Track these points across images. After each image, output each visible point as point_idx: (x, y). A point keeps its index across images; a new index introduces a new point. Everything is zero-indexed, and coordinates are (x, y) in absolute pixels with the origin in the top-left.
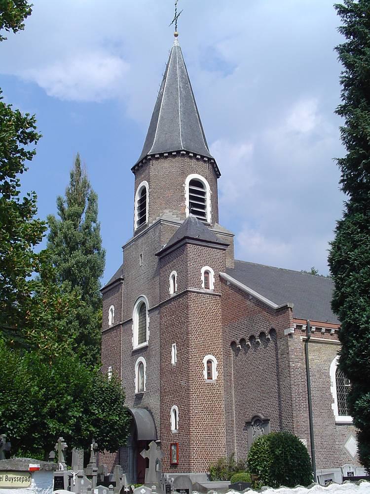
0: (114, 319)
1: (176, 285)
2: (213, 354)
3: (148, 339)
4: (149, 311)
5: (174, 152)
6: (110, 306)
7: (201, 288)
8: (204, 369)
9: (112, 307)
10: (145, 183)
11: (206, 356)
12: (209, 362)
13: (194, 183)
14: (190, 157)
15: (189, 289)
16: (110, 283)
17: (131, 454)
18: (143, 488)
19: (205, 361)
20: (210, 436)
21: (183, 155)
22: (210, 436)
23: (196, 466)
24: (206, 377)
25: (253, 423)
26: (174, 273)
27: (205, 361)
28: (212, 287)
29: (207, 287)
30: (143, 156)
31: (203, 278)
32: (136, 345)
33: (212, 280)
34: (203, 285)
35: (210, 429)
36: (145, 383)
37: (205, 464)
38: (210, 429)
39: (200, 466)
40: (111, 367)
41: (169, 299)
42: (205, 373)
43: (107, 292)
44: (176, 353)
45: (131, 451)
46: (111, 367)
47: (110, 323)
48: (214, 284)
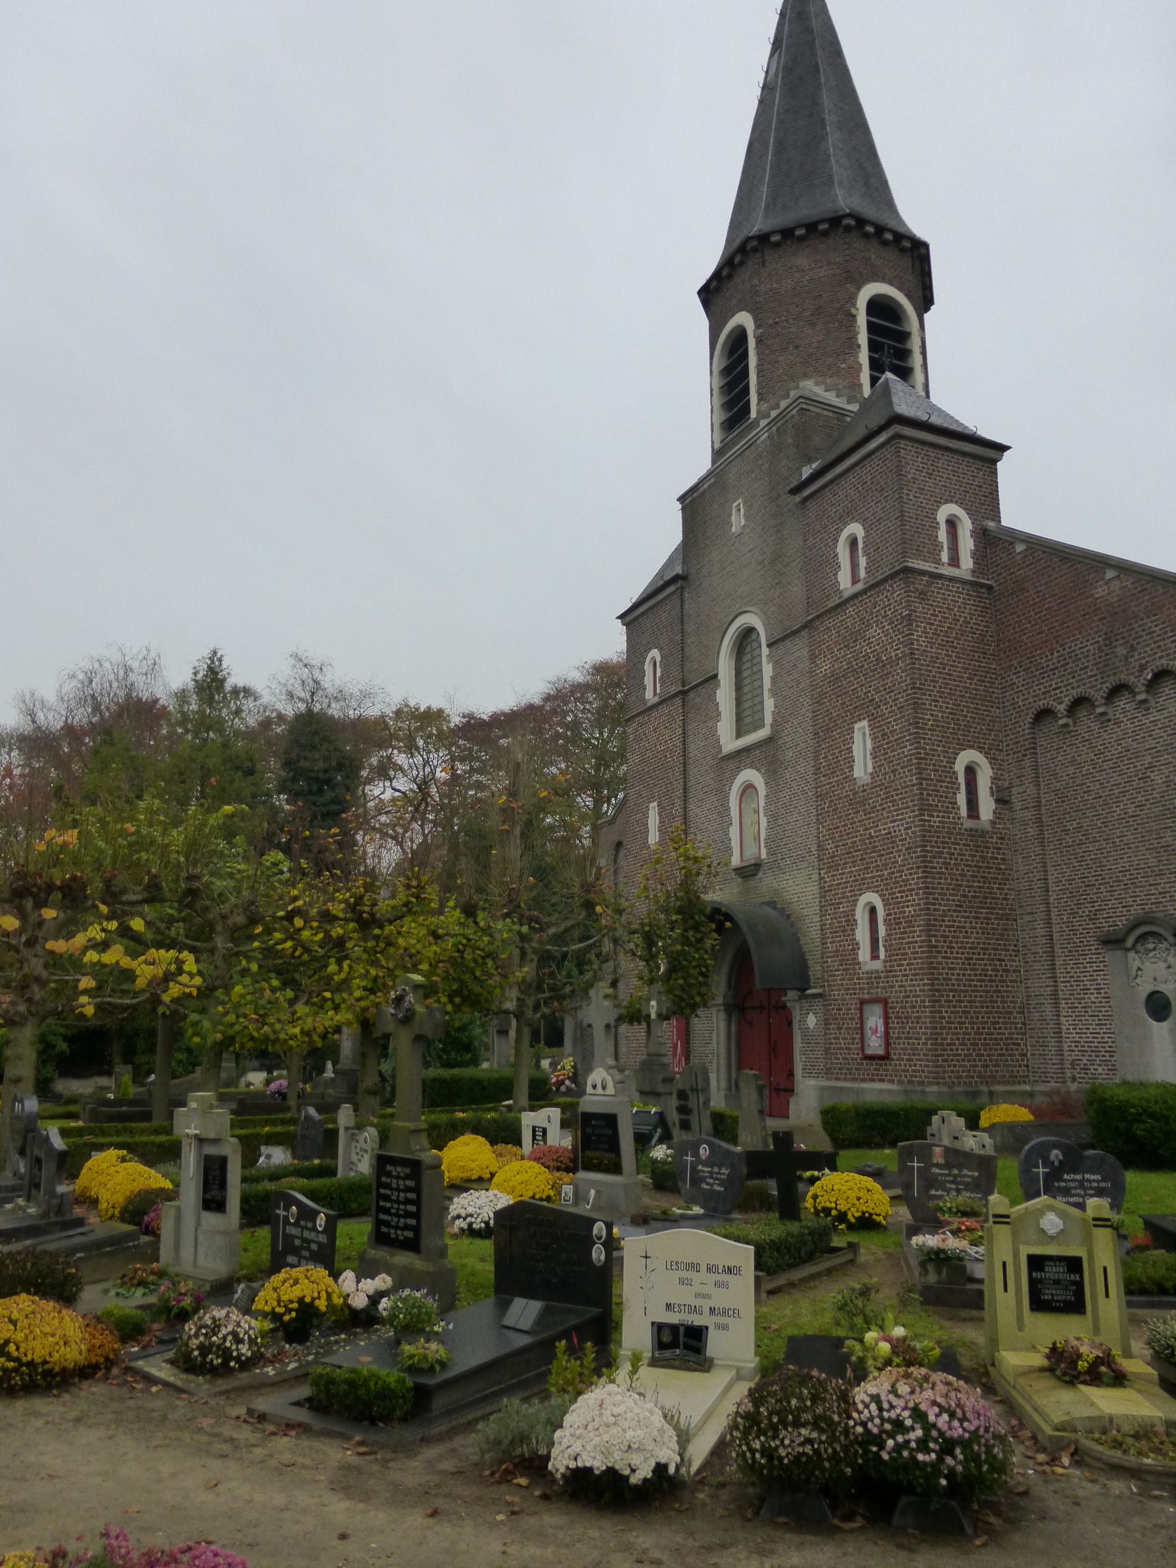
0: (663, 682)
1: (863, 561)
2: (980, 749)
3: (768, 719)
4: (769, 646)
5: (822, 221)
6: (650, 649)
7: (938, 562)
8: (958, 789)
9: (655, 653)
10: (744, 319)
11: (962, 753)
12: (970, 771)
13: (878, 306)
14: (867, 236)
15: (910, 564)
16: (650, 591)
17: (723, 1025)
18: (1051, 1208)
19: (960, 767)
20: (983, 981)
21: (848, 229)
22: (983, 981)
23: (949, 1066)
24: (964, 812)
25: (1129, 942)
26: (856, 529)
27: (960, 767)
28: (967, 562)
29: (955, 561)
30: (737, 243)
31: (942, 536)
32: (729, 742)
33: (967, 544)
34: (945, 557)
35: (983, 959)
36: (763, 836)
37: (957, 1050)
38: (983, 959)
39: (960, 1066)
40: (655, 804)
41: (838, 601)
42: (961, 799)
43: (636, 618)
44: (869, 746)
45: (722, 1015)
46: (655, 804)
47: (649, 694)
48: (974, 555)
